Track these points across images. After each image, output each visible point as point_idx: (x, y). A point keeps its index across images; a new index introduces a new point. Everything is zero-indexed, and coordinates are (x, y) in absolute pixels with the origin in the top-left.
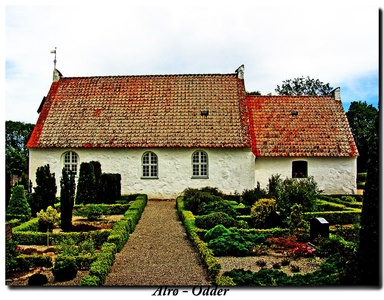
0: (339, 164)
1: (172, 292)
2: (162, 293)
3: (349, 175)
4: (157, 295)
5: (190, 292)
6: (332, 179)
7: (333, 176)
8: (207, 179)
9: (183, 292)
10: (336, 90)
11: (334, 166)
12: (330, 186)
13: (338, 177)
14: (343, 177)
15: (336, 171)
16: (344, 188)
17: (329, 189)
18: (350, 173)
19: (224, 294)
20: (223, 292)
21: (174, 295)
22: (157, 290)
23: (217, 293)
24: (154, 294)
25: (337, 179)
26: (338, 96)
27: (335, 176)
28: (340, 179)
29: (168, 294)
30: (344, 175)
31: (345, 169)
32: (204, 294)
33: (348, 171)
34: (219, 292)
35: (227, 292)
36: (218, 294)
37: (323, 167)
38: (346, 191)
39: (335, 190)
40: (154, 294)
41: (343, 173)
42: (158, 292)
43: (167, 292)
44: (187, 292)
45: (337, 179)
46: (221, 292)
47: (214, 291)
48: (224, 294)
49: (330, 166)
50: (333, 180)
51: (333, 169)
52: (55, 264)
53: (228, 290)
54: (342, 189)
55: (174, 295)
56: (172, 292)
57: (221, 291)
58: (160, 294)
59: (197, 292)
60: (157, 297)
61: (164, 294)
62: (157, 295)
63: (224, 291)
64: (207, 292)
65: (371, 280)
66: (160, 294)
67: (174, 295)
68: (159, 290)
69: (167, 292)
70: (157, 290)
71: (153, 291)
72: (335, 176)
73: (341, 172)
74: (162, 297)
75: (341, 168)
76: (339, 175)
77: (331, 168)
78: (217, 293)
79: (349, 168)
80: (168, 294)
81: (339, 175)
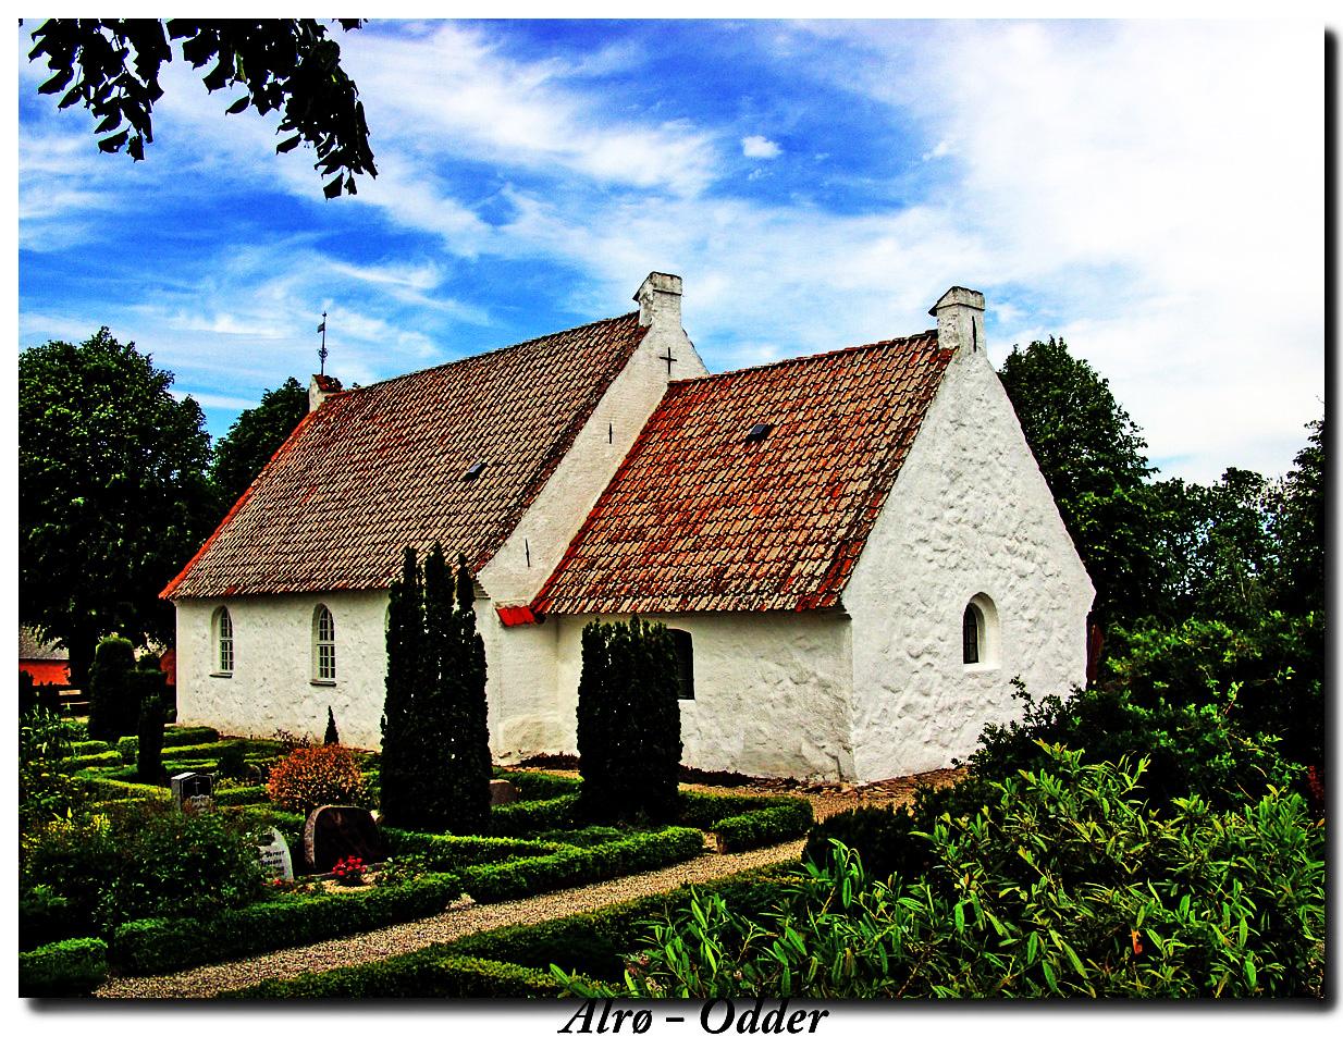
0: (792, 643)
1: (628, 1022)
2: (594, 1025)
3: (828, 694)
4: (575, 1032)
5: (693, 1020)
6: (768, 706)
7: (772, 696)
8: (327, 689)
9: (668, 1020)
10: (941, 304)
11: (774, 651)
12: (762, 738)
13: (788, 699)
14: (806, 703)
15: (782, 673)
16: (807, 750)
17: (756, 748)
18: (829, 687)
19: (812, 1029)
20: (808, 1021)
21: (636, 1030)
22: (577, 1016)
23: (784, 1024)
24: (566, 1030)
25: (783, 711)
26: (950, 328)
27: (776, 695)
28: (793, 711)
29: (616, 1030)
30: (810, 690)
31: (810, 668)
32: (740, 1030)
33: (821, 674)
34: (792, 1021)
35: (823, 1021)
36: (791, 1030)
37: (740, 655)
38: (814, 763)
39: (775, 755)
40: (566, 1030)
41: (805, 683)
42: (579, 1023)
43: (611, 1022)
44: (681, 1020)
45: (783, 711)
46: (799, 1021)
47: (774, 1018)
48: (812, 1029)
49: (762, 653)
50: (772, 712)
51: (773, 666)
52: (1202, 619)
53: (826, 1014)
54: (799, 756)
55: (636, 1030)
56: (628, 1022)
57: (802, 1019)
58: (586, 1029)
59: (716, 1020)
60: (576, 1039)
61: (601, 1030)
62: (575, 1032)
63: (812, 1016)
64: (754, 1022)
65: (1297, 985)
66: (586, 1029)
67: (636, 1030)
68: (584, 1013)
69: (611, 1022)
70: (577, 1016)
71: (561, 1019)
72: (776, 695)
73: (796, 679)
74: (593, 1038)
75: (798, 659)
76: (793, 691)
77: (762, 662)
78: (784, 1024)
79: (824, 661)
80: (616, 1030)
81: (793, 691)
